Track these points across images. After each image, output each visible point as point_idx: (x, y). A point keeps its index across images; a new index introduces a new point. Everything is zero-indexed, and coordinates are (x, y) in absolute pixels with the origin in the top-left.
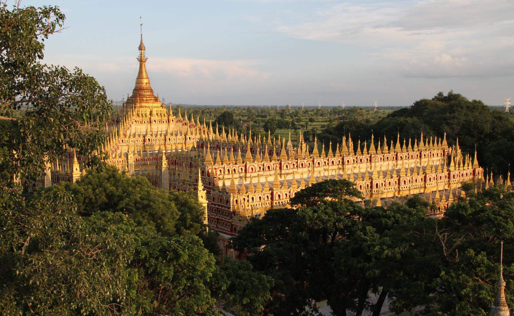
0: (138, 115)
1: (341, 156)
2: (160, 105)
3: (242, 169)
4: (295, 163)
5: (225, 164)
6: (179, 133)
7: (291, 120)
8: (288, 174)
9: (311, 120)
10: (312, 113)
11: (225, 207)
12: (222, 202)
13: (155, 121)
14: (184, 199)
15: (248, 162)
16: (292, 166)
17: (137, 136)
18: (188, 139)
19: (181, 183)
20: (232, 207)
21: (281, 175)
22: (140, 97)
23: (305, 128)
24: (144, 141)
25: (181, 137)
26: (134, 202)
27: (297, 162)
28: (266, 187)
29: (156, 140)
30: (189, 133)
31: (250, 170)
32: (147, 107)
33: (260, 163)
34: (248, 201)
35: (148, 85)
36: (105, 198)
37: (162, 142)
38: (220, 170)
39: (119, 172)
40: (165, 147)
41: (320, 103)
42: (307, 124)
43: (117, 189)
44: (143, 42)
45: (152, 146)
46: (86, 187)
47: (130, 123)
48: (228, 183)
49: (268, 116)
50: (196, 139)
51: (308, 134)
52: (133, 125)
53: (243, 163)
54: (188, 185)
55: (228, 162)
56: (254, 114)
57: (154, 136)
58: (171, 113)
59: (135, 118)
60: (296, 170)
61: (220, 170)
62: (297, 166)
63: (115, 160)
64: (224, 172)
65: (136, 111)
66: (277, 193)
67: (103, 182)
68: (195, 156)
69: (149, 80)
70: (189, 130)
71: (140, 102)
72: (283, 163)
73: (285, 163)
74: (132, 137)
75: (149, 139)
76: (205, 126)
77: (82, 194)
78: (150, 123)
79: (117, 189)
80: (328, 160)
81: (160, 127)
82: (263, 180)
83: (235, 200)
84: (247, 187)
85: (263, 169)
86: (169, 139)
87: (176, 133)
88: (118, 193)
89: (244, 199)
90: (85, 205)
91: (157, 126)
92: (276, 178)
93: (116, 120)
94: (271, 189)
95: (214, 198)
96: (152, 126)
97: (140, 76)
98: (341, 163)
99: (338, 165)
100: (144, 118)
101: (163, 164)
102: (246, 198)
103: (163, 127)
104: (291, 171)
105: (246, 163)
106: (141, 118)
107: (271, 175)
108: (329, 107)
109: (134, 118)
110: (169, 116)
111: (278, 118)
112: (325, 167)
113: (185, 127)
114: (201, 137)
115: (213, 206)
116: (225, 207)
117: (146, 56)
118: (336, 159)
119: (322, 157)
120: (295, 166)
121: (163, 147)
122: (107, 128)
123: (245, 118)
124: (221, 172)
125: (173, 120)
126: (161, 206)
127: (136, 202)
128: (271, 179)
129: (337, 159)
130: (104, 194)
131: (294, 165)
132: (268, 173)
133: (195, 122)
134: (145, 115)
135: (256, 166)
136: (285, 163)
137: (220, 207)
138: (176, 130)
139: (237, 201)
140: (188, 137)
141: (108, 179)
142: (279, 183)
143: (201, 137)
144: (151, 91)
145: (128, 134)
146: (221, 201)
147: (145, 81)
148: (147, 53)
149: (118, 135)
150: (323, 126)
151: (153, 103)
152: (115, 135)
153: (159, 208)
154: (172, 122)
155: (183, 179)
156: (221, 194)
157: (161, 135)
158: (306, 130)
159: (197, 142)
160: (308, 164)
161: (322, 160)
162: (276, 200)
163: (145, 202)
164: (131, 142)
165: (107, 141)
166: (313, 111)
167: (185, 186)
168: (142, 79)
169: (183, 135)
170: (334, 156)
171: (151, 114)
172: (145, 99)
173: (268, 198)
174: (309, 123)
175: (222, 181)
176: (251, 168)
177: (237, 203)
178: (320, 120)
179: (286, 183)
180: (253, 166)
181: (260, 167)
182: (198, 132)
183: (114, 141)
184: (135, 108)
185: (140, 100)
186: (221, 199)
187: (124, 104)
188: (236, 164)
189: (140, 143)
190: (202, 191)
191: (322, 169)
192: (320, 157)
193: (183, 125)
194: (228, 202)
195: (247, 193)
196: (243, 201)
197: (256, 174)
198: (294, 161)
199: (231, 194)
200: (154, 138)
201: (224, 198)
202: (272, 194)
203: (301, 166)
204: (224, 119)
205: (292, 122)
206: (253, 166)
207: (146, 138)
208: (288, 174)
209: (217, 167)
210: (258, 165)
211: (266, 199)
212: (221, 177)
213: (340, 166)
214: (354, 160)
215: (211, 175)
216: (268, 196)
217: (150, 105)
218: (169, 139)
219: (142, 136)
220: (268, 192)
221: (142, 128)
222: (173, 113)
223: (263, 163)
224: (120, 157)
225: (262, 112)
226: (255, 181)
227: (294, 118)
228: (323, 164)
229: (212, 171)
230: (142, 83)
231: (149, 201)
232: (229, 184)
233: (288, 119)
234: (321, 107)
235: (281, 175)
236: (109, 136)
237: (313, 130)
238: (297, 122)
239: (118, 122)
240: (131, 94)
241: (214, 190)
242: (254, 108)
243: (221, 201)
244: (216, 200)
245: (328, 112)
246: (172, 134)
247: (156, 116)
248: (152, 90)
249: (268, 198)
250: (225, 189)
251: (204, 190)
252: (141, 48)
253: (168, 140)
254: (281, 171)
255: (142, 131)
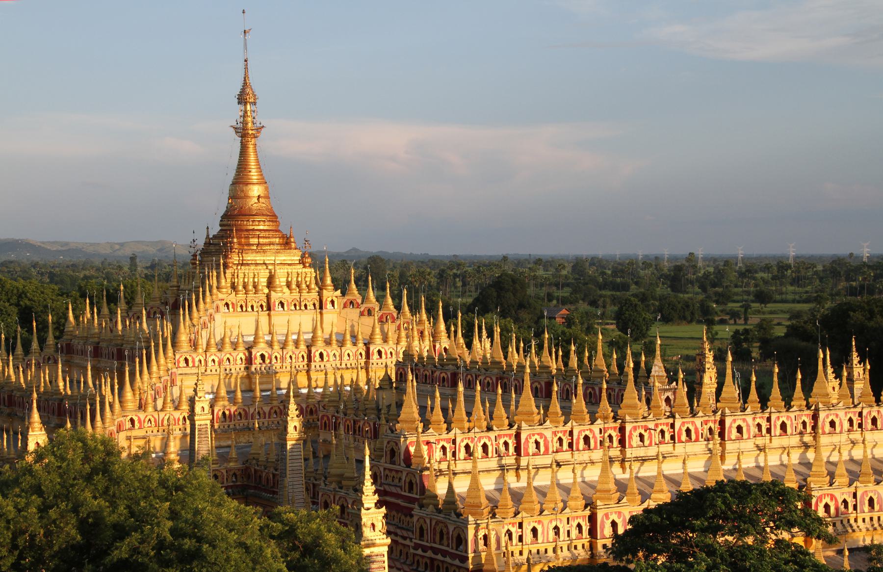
0: (234, 287)
1: (808, 407)
2: (297, 258)
3: (506, 444)
4: (665, 428)
5: (456, 431)
6: (348, 337)
7: (701, 297)
8: (643, 460)
9: (762, 297)
10: (765, 275)
11: (454, 556)
12: (445, 541)
13: (282, 304)
14: (309, 534)
15: (524, 425)
16: (657, 437)
17: (228, 348)
18: (376, 356)
19: (334, 485)
20: (471, 555)
21: (623, 462)
22: (239, 238)
23: (742, 321)
24: (249, 360)
25: (354, 349)
26: (154, 542)
27: (673, 426)
28: (576, 499)
29: (283, 359)
30: (378, 338)
31: (532, 448)
32: (266, 262)
33: (561, 428)
34: (521, 539)
35: (263, 204)
36: (73, 532)
37: (302, 364)
38: (444, 448)
39: (124, 455)
40: (309, 379)
41: (790, 248)
42: (747, 307)
43: (113, 505)
44: (251, 81)
45: (270, 374)
46: (22, 502)
47: (211, 311)
48: (461, 486)
49: (633, 287)
50: (397, 354)
51: (746, 340)
52: (218, 317)
53: (511, 426)
54: (351, 491)
55: (467, 425)
56: (593, 280)
57: (276, 347)
58: (329, 281)
59: (225, 295)
60: (666, 448)
61: (444, 448)
62: (673, 438)
63: (162, 415)
64: (454, 454)
65: (229, 275)
66: (607, 516)
67: (72, 486)
68: (389, 406)
69: (267, 189)
70: (378, 330)
71: (241, 252)
72: (628, 427)
73: (635, 428)
74: (213, 350)
75: (263, 356)
76: (424, 317)
77: (8, 522)
78: (269, 309)
79: (113, 505)
80: (769, 420)
81: (295, 322)
82: (565, 476)
83: (481, 534)
84: (517, 497)
85: (571, 445)
86: (321, 355)
87: (341, 339)
88: (112, 519)
89: (509, 534)
90: (16, 553)
91: (286, 319)
92: (604, 471)
93: (171, 301)
94: (590, 504)
95: (421, 529)
96: (325, 316)
97: (240, 178)
98: (809, 429)
99: (801, 433)
100: (251, 295)
101: (290, 429)
102: (514, 530)
103: (304, 321)
104: (652, 451)
105: (519, 428)
106: (241, 296)
107: (593, 463)
108: (821, 258)
109: (221, 296)
110: (321, 289)
111: (662, 290)
112: (760, 441)
113: (368, 321)
114: (409, 347)
115: (420, 552)
116: (454, 556)
117: (258, 120)
118: (792, 415)
119: (749, 411)
120: (667, 436)
121: (302, 380)
122: (145, 325)
123: (565, 292)
124: (445, 453)
125: (332, 302)
126: (235, 554)
127: (161, 545)
128: (593, 474)
129: (797, 416)
130: (74, 521)
131: (662, 432)
132: (585, 456)
133: (398, 308)
134: (255, 287)
135: (548, 434)
136: (635, 428)
137: (439, 557)
138: (341, 330)
139: (486, 537)
140: (374, 349)
141: (89, 478)
142: (612, 487)
143: (409, 347)
144: (273, 217)
145: (203, 342)
146: (441, 538)
147: (255, 191)
148: (261, 114)
149: (174, 345)
150: (796, 315)
151: (278, 252)
152: (165, 346)
153: (228, 560)
154: (329, 306)
155: (339, 471)
156: (441, 517)
157: (297, 343)
158: (741, 328)
159: (398, 364)
160: (706, 432)
161: (749, 419)
162: (604, 537)
163: (188, 544)
164: (210, 363)
165: (141, 363)
166: (767, 268)
167: (342, 493)
168: (247, 184)
169: (361, 345)
170: (788, 407)
171: (270, 283)
172: (255, 241)
173: (580, 531)
174: (756, 306)
175: (447, 479)
176: (533, 440)
177: (486, 544)
178: (790, 297)
179: (634, 487)
180: (541, 435)
181: (560, 440)
182: (403, 334)
183: (161, 365)
184: (226, 266)
185: (240, 244)
186: (441, 533)
187: (195, 255)
188: (489, 429)
189: (238, 368)
190: (373, 510)
191: (748, 445)
192: (744, 410)
193: (362, 314)
194: (461, 540)
195: (516, 514)
196: (504, 539)
197: (547, 460)
198: (664, 421)
199: (471, 518)
200: (277, 351)
201: (451, 528)
202: (592, 519)
203: (684, 437)
204: (499, 296)
205: (702, 303)
206: (541, 435)
207: (254, 352)
208: (643, 460)
209: (432, 440)
210: (555, 433)
211: (574, 533)
212: (444, 466)
213: (808, 439)
214: (851, 421)
215: (413, 460)
216: (579, 526)
217: (269, 258)
218: (321, 355)
219: (241, 348)
220: (580, 513)
221: (243, 325)
222: (333, 280)
223: (568, 427)
224: (177, 408)
225: (615, 273)
226: (543, 479)
227: (711, 291)
228: (754, 430)
229: (418, 449)
230: (247, 197)
231: (199, 540)
232: (465, 489)
233: (693, 294)
234: (796, 258)
235: (623, 462)
236: (148, 348)
237: (760, 326)
238: (717, 302)
239: (176, 307)
240: (215, 229)
241: (421, 506)
242: (595, 261)
243: (441, 538)
244: (428, 535)
245: (816, 273)
246: (328, 342)
247: (286, 290)
248: (275, 216)
249: (580, 531)
250: (454, 503)
251: (379, 505)
252: (242, 99)
253: (318, 358)
254: (623, 452)
255: (303, 329)
